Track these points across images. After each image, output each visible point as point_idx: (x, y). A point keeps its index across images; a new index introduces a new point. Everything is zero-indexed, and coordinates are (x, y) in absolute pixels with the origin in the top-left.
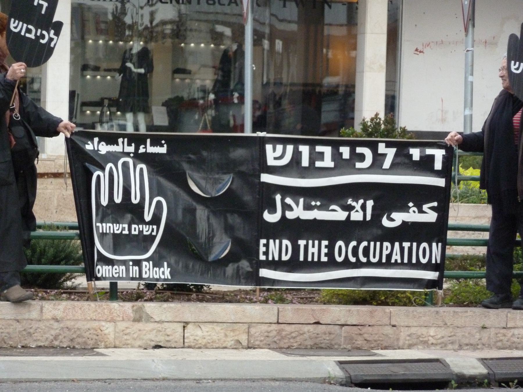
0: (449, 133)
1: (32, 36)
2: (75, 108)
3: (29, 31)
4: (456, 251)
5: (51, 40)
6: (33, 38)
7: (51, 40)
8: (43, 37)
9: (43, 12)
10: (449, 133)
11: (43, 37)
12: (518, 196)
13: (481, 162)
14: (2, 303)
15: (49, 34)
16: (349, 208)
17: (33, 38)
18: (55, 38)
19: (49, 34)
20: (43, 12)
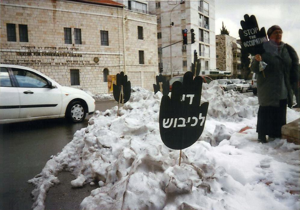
0: (199, 29)
1: (184, 125)
2: (154, 16)
3: (180, 122)
4: (229, 52)
5: (200, 121)
6: (185, 126)
7: (200, 121)
8: (193, 121)
9: (191, 103)
10: (199, 29)
11: (193, 121)
12: (250, 64)
13: (240, 59)
14: (1, 109)
15: (198, 118)
16: (255, 78)
17: (185, 126)
18: (203, 118)
19: (198, 118)
20: (191, 103)
